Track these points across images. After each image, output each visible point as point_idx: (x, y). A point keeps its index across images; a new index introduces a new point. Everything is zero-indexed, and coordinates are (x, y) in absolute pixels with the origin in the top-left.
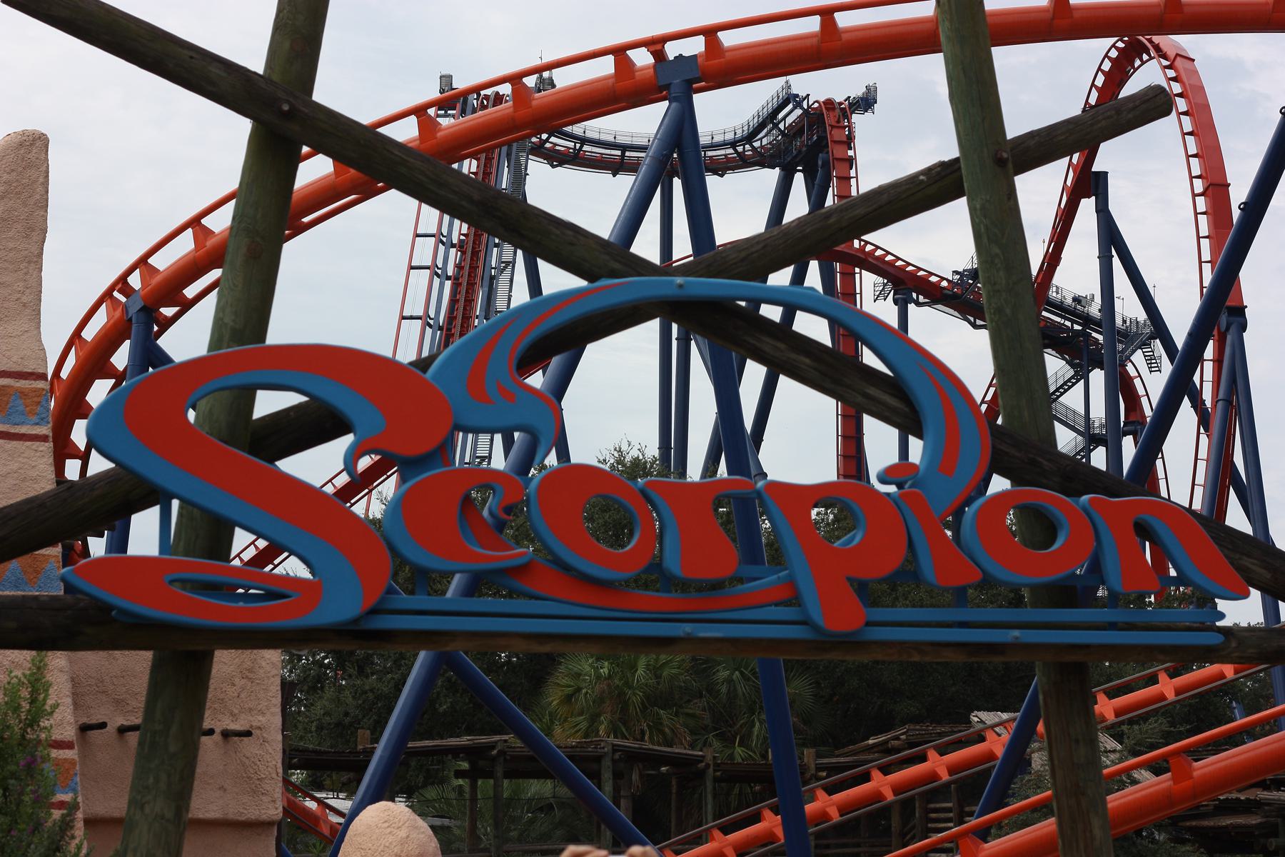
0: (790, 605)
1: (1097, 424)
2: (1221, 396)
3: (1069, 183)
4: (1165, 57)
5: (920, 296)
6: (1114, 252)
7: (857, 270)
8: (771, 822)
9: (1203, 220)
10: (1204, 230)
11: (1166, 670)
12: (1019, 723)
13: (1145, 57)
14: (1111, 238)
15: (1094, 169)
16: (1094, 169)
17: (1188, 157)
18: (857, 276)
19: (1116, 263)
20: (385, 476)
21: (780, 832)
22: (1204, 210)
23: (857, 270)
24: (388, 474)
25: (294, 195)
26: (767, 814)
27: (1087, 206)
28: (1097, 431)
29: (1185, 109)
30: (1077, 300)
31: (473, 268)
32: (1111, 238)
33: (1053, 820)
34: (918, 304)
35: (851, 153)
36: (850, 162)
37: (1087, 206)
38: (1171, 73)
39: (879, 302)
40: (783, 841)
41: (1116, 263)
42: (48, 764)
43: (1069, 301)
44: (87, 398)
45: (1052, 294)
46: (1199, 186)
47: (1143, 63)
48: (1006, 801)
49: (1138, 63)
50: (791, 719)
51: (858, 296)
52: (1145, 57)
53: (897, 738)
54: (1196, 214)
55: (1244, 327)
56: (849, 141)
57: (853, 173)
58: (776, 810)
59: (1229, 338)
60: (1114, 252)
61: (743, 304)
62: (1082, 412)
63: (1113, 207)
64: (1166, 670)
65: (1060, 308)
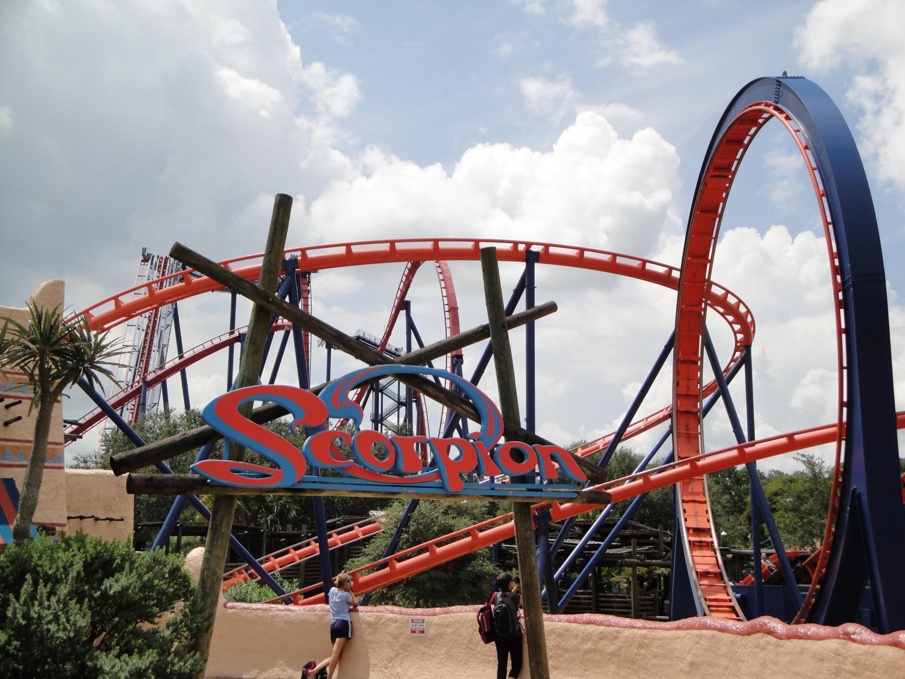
0: (165, 410)
1: (402, 398)
3: (396, 304)
6: (412, 332)
7: (310, 334)
8: (315, 546)
9: (448, 321)
10: (448, 325)
12: (131, 430)
14: (411, 326)
17: (442, 288)
18: (310, 337)
19: (413, 335)
20: (713, 240)
21: (318, 549)
22: (447, 303)
23: (310, 334)
26: (313, 543)
27: (403, 313)
28: (402, 401)
29: (442, 278)
30: (396, 350)
31: (154, 327)
32: (411, 326)
33: (470, 537)
34: (335, 349)
35: (309, 288)
36: (308, 292)
37: (403, 313)
38: (439, 270)
39: (320, 347)
40: (318, 553)
41: (413, 335)
43: (393, 350)
45: (387, 347)
46: (447, 308)
47: (730, 324)
48: (164, 546)
51: (310, 345)
53: (339, 521)
54: (443, 297)
56: (308, 283)
57: (309, 296)
58: (316, 541)
60: (412, 332)
62: (397, 393)
63: (412, 314)
65: (390, 352)
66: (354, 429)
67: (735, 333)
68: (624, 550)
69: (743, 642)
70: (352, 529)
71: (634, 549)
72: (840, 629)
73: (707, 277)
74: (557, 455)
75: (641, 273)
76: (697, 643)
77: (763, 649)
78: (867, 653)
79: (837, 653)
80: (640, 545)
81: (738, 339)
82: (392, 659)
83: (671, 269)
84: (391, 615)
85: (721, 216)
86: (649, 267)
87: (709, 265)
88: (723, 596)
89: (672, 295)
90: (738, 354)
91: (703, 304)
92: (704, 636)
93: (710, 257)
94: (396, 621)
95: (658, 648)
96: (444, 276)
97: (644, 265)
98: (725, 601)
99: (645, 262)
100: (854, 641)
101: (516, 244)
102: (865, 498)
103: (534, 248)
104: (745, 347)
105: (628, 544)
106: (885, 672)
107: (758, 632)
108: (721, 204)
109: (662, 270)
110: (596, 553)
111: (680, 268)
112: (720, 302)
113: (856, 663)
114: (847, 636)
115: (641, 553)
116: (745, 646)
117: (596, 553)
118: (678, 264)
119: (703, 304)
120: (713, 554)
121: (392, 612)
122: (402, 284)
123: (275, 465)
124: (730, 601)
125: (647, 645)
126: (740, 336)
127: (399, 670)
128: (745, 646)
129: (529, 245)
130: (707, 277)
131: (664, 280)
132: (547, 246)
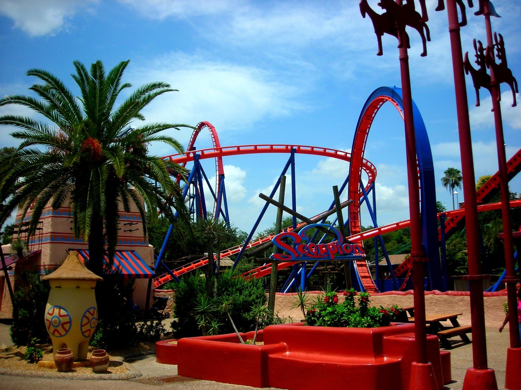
2: (220, 191)
4: (209, 126)
5: (158, 183)
11: (167, 274)
13: (205, 126)
15: (193, 146)
16: (193, 146)
20: (364, 143)
24: (365, 141)
25: (397, 3)
42: (390, 244)
44: (349, 163)
47: (368, 173)
49: (203, 127)
50: (286, 250)
52: (205, 126)
53: (189, 257)
55: (224, 178)
59: (221, 181)
61: (417, 163)
64: (167, 274)
66: (224, 225)
67: (369, 177)
68: (322, 268)
69: (404, 297)
70: (199, 261)
71: (326, 267)
72: (432, 291)
73: (362, 157)
74: (358, 248)
75: (335, 155)
76: (390, 298)
77: (410, 299)
78: (439, 297)
79: (431, 298)
80: (328, 265)
81: (369, 175)
82: (280, 310)
83: (347, 153)
84: (279, 296)
85: (368, 134)
86: (338, 153)
87: (362, 153)
88: (372, 285)
89: (347, 164)
90: (369, 184)
91: (360, 168)
92: (392, 296)
93: (363, 150)
94: (281, 297)
95: (377, 301)
96: (214, 135)
97: (337, 153)
98: (373, 286)
99: (337, 151)
100: (436, 294)
101: (287, 146)
102: (426, 248)
103: (294, 148)
104: (372, 182)
105: (323, 266)
106: (444, 302)
107: (409, 294)
108: (368, 129)
109: (343, 154)
110: (313, 268)
111: (351, 153)
112: (365, 165)
113: (436, 300)
114: (434, 293)
115: (329, 268)
116: (405, 298)
117: (313, 268)
118: (350, 151)
119: (360, 168)
120: (366, 269)
121: (279, 295)
122: (192, 139)
123: (290, 254)
124: (374, 286)
125: (374, 300)
126: (371, 178)
127: (283, 313)
128: (405, 298)
129: (292, 146)
130: (362, 157)
131: (344, 158)
132: (299, 147)
